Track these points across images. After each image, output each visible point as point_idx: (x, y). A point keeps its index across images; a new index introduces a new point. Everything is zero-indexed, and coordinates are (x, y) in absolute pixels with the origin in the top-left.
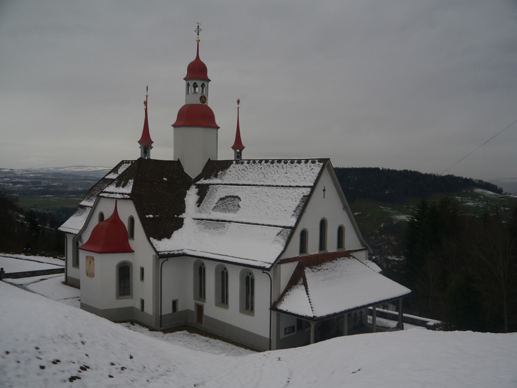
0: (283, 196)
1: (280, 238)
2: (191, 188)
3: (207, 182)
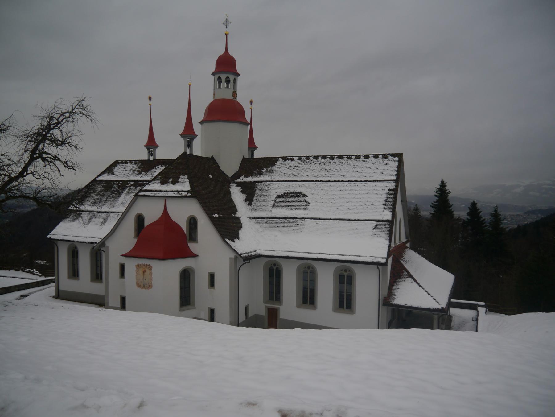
0: (361, 190)
1: (378, 231)
2: (231, 186)
3: (249, 179)
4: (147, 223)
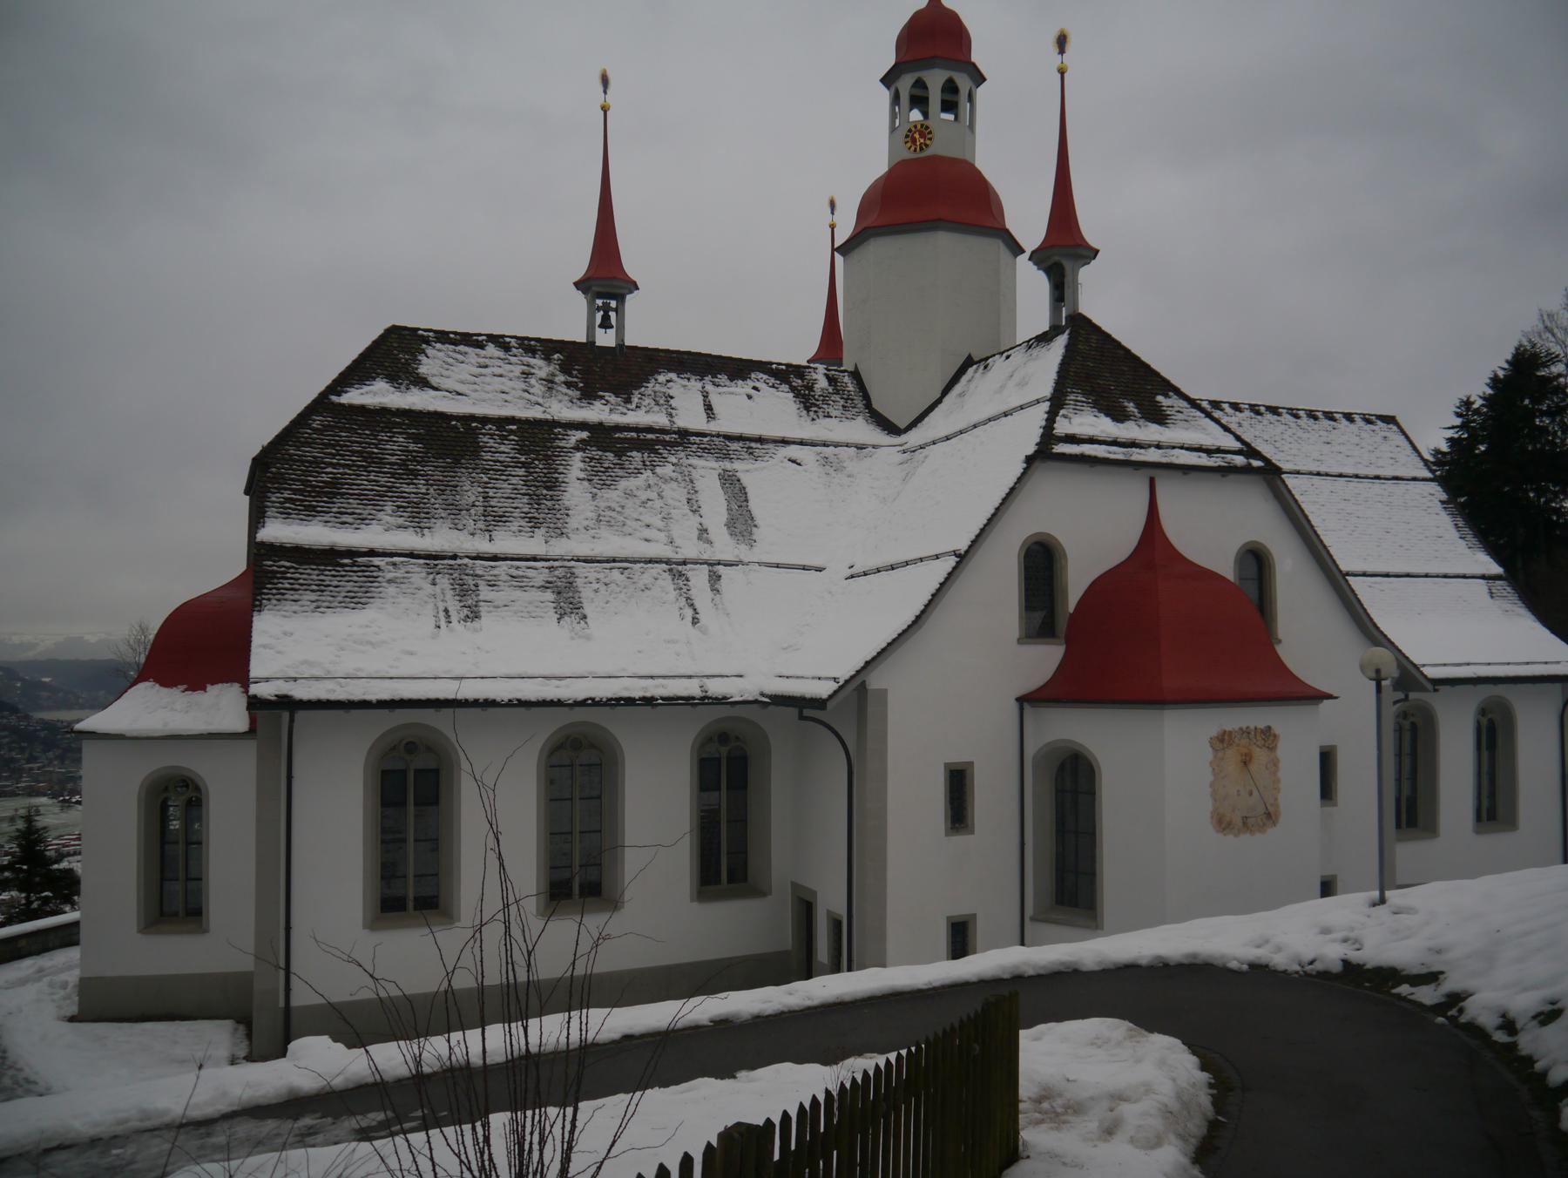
4: (1076, 582)
